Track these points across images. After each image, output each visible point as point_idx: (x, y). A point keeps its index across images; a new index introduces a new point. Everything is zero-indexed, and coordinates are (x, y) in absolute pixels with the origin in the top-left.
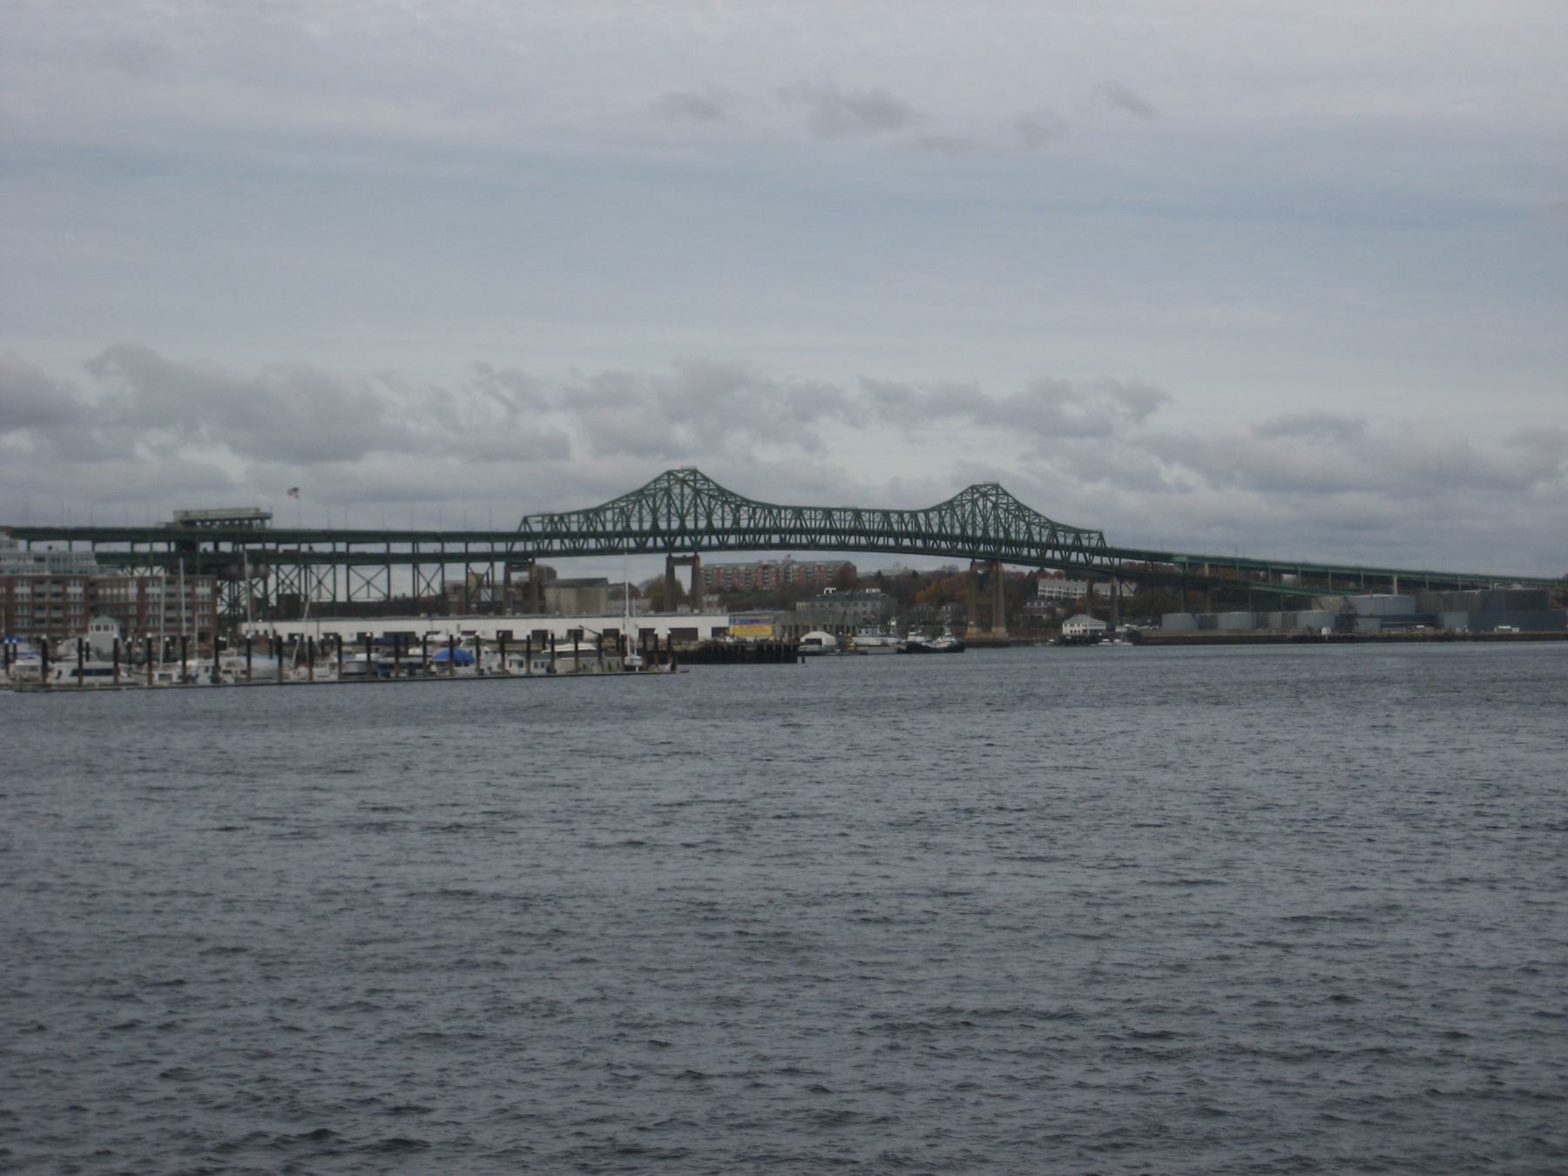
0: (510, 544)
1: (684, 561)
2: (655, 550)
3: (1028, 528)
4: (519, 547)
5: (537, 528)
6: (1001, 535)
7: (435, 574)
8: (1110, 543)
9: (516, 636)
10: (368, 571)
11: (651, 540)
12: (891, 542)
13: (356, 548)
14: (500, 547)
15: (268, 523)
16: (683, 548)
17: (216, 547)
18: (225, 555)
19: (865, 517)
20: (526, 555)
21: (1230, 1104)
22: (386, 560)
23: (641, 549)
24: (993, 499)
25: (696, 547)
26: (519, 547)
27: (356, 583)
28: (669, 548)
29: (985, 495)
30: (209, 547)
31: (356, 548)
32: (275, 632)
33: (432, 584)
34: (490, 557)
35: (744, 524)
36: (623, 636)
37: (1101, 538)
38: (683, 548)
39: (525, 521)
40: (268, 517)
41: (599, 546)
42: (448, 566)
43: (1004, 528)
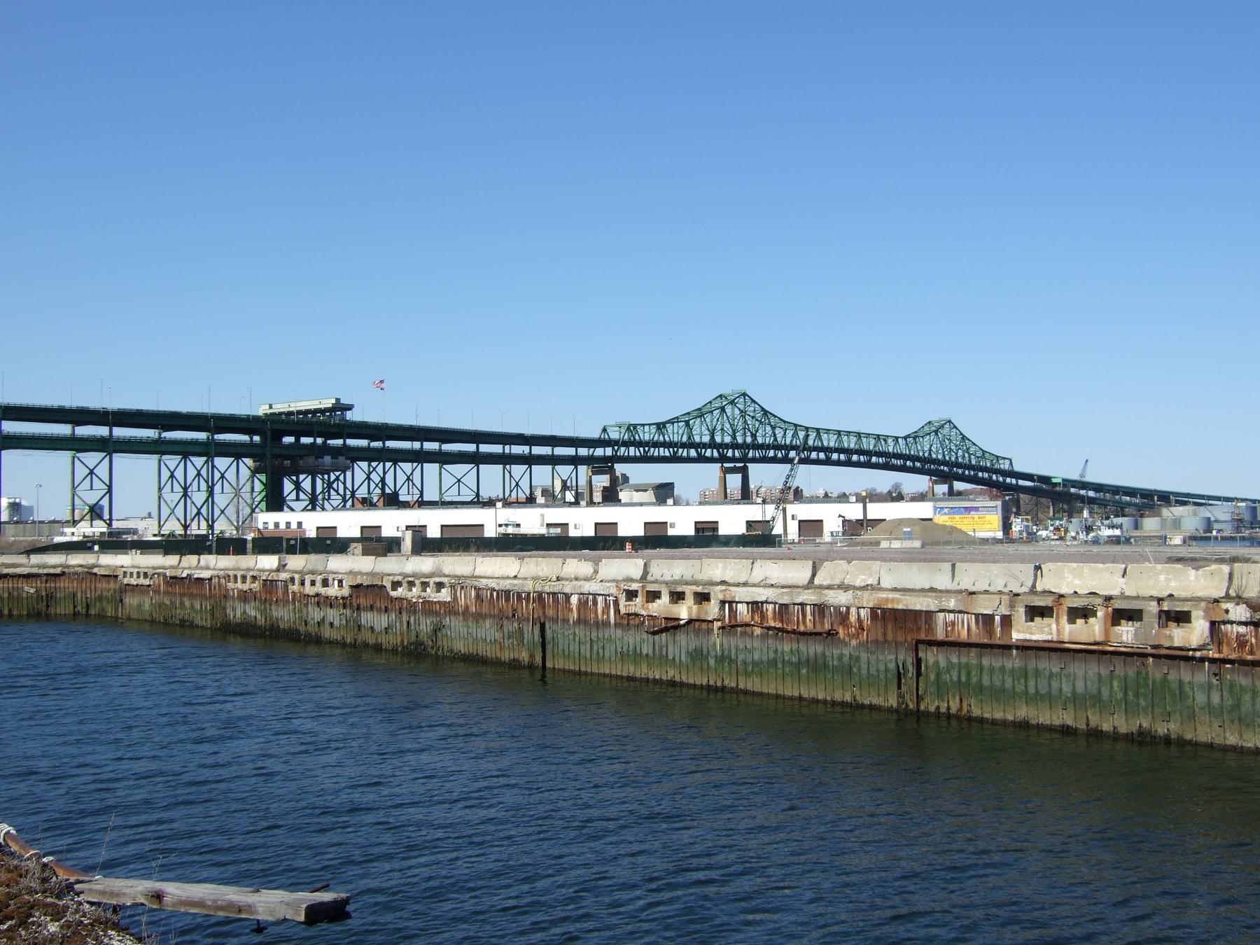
0: (592, 450)
1: (734, 470)
2: (711, 460)
3: (969, 457)
4: (599, 452)
5: (614, 435)
6: (749, 440)
7: (180, 461)
8: (1018, 468)
9: (723, 531)
10: (459, 469)
11: (730, 451)
12: (822, 456)
13: (448, 447)
14: (583, 452)
15: (349, 416)
16: (733, 460)
17: (251, 438)
18: (305, 446)
19: (824, 437)
20: (605, 459)
21: (499, 930)
22: (477, 459)
23: (701, 459)
24: (741, 407)
25: (744, 459)
26: (599, 452)
27: (448, 480)
28: (722, 459)
29: (732, 402)
30: (291, 439)
31: (448, 447)
32: (300, 524)
33: (202, 472)
34: (575, 461)
35: (810, 443)
36: (697, 530)
37: (1011, 463)
38: (733, 460)
39: (604, 430)
40: (350, 407)
41: (638, 454)
42: (484, 468)
43: (751, 433)
